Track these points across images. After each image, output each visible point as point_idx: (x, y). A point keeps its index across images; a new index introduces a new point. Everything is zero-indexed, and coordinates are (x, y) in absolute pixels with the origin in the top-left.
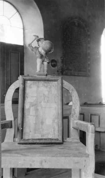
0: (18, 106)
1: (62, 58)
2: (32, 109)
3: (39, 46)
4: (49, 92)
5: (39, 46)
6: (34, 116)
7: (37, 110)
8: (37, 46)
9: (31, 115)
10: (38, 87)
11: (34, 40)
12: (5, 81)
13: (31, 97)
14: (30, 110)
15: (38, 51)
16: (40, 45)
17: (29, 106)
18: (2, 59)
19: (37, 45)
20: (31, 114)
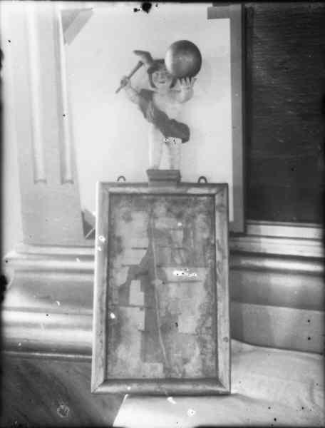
0: (94, 242)
1: (178, 261)
2: (136, 286)
3: (153, 86)
4: (186, 231)
5: (153, 86)
6: (141, 309)
7: (149, 289)
8: (150, 88)
9: (134, 306)
10: (153, 216)
11: (134, 71)
12: (75, 358)
13: (134, 248)
14: (128, 288)
15: (150, 106)
16: (156, 84)
17: (126, 275)
18: (67, 277)
19: (149, 84)
20: (132, 301)
